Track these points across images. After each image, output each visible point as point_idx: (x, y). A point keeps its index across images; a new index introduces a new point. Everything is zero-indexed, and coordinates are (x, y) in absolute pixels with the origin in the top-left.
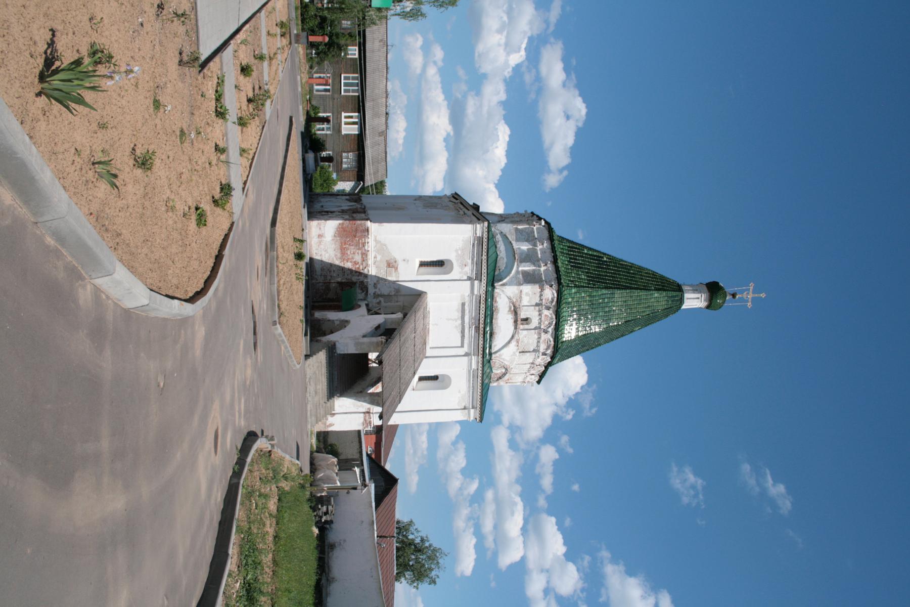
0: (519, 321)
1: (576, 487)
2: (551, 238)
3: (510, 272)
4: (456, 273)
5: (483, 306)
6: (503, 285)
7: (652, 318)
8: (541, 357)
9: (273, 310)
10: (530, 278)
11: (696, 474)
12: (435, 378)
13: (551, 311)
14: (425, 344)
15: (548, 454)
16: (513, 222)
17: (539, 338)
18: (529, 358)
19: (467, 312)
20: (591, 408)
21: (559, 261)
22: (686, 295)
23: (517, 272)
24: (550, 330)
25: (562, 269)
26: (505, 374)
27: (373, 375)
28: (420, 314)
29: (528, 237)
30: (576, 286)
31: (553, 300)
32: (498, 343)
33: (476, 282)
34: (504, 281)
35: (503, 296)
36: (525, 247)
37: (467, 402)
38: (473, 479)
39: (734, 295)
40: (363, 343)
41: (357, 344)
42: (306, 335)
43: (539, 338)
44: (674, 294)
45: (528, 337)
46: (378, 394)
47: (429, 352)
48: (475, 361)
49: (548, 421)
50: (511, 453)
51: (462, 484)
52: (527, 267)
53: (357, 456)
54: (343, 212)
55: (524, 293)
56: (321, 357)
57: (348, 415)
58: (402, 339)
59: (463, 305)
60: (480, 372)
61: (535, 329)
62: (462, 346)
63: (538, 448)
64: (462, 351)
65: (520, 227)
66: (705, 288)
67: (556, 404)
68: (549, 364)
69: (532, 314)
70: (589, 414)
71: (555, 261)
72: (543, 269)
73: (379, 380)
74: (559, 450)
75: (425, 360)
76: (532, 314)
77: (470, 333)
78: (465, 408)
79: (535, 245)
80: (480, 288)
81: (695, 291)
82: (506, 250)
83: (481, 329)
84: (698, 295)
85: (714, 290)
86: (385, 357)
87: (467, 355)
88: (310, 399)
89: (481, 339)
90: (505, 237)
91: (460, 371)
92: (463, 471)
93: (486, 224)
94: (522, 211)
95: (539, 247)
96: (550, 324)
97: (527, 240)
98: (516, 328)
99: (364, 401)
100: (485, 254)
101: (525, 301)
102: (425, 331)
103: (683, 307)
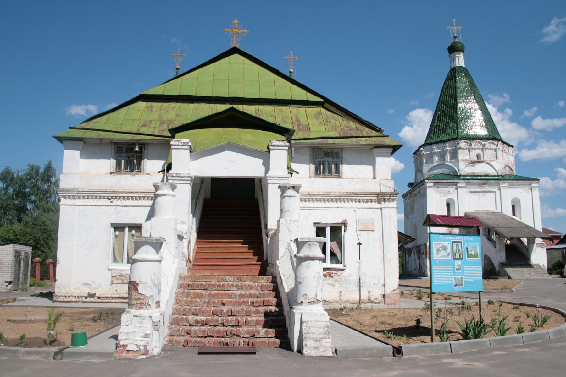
0: (479, 160)
1: (561, 104)
2: (431, 144)
3: (451, 166)
4: (454, 196)
5: (471, 181)
6: (459, 170)
7: (472, 84)
8: (499, 147)
9: (505, 292)
10: (454, 155)
11: (547, 24)
12: (513, 207)
13: (473, 143)
14: (494, 213)
15: (539, 123)
16: (421, 165)
17: (488, 148)
18: (499, 153)
19: (475, 190)
20: (503, 97)
21: (443, 139)
22: (457, 65)
23: (451, 162)
24: (483, 143)
25: (448, 137)
26: (509, 167)
27: (515, 242)
28: (479, 216)
29: (430, 157)
30: (457, 129)
31: (467, 142)
32: (492, 172)
33: (459, 185)
34: (456, 169)
35: (465, 170)
36: (436, 158)
37: (527, 188)
38: (558, 171)
39: (455, 37)
40: (500, 248)
41: (500, 251)
42: (497, 278)
43: (488, 148)
44: (457, 72)
45: (488, 155)
46: (528, 239)
47: (499, 210)
48: (503, 184)
49: (514, 124)
50: (538, 148)
51: (562, 179)
52: (448, 157)
53: (560, 252)
54: (419, 258)
55: (463, 158)
56: (509, 270)
57: (539, 256)
58: (496, 226)
59: (471, 192)
60: (509, 181)
61: (483, 151)
62: (495, 192)
63: (534, 130)
64: (498, 192)
65: (425, 161)
66: (452, 54)
67: (503, 120)
68: (504, 143)
69: (474, 153)
70: (508, 98)
71: (444, 142)
72: (448, 148)
73: (519, 239)
74: (535, 116)
75: (504, 212)
76: (474, 153)
77: (487, 188)
78: (531, 189)
79: (435, 153)
80: (461, 183)
81: (454, 60)
82: (438, 169)
83: (485, 181)
84: (457, 58)
85: (453, 49)
86: (509, 236)
87: (499, 189)
88: (534, 277)
89: (490, 181)
90: (431, 170)
91: (509, 193)
92: (553, 179)
93: (426, 181)
94: (413, 160)
95: (436, 150)
96: (480, 143)
97: (432, 157)
98: (483, 162)
99: (533, 247)
100: (443, 181)
101: (467, 157)
102: (487, 213)
103: (464, 66)
